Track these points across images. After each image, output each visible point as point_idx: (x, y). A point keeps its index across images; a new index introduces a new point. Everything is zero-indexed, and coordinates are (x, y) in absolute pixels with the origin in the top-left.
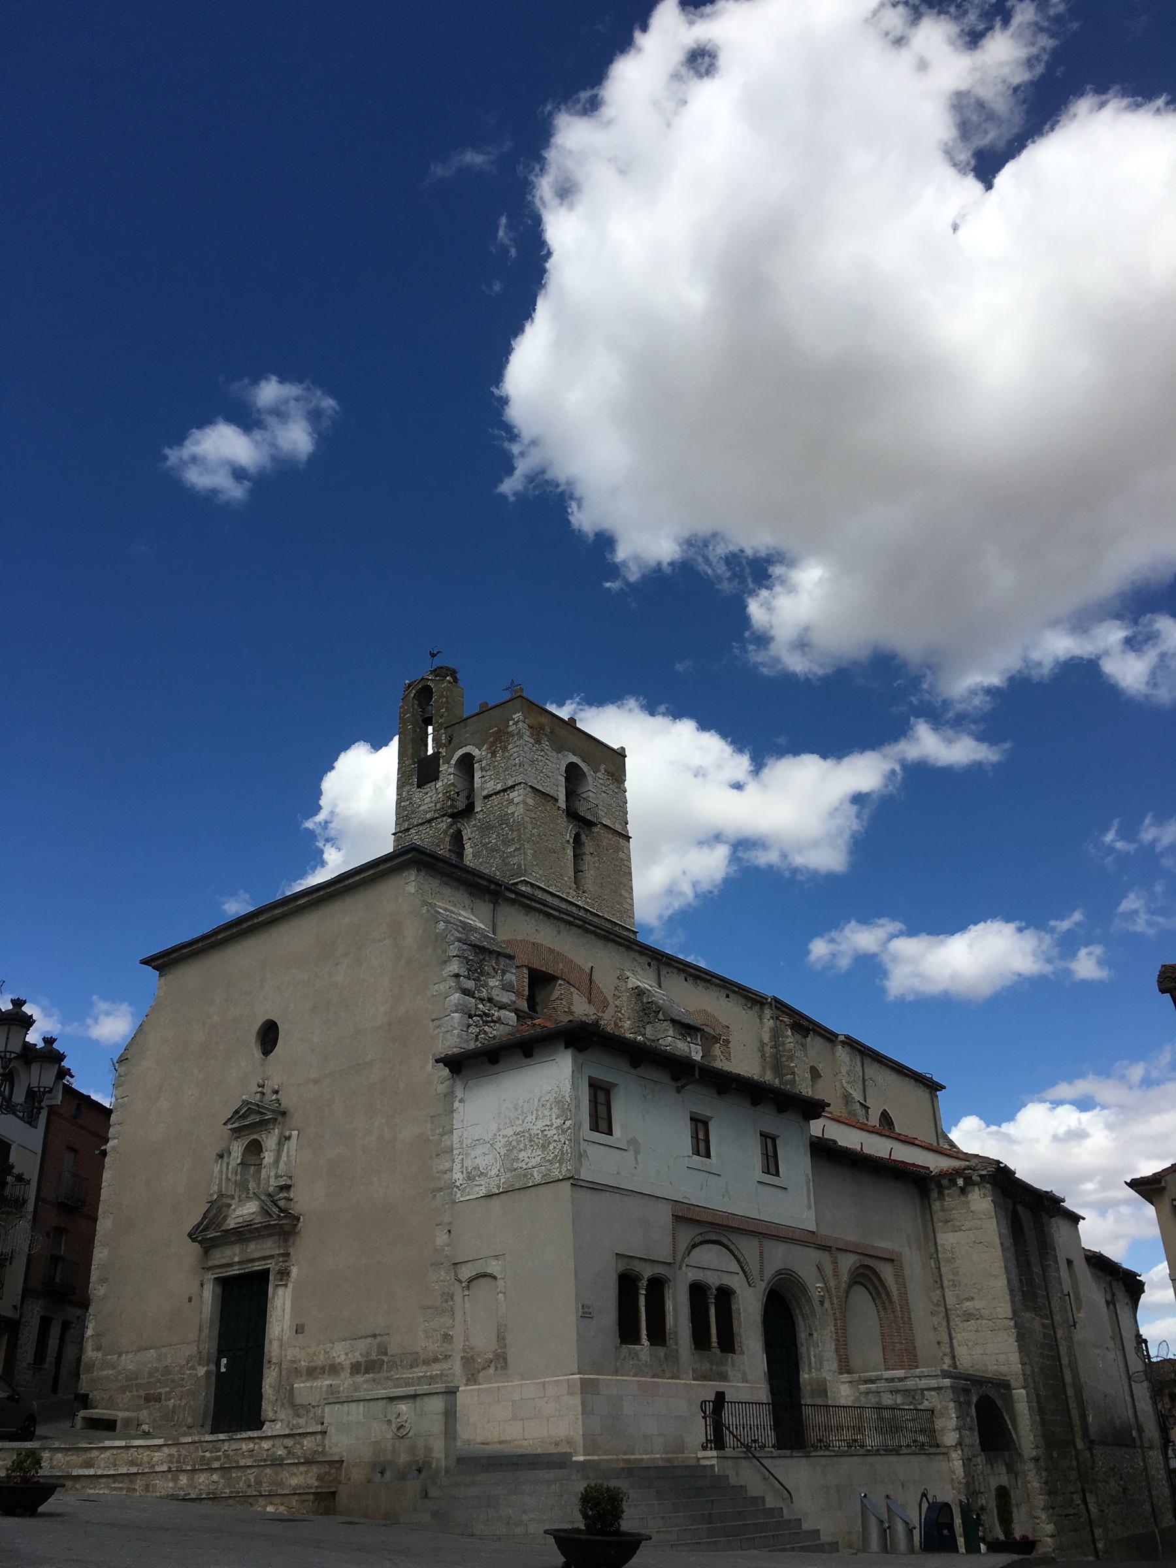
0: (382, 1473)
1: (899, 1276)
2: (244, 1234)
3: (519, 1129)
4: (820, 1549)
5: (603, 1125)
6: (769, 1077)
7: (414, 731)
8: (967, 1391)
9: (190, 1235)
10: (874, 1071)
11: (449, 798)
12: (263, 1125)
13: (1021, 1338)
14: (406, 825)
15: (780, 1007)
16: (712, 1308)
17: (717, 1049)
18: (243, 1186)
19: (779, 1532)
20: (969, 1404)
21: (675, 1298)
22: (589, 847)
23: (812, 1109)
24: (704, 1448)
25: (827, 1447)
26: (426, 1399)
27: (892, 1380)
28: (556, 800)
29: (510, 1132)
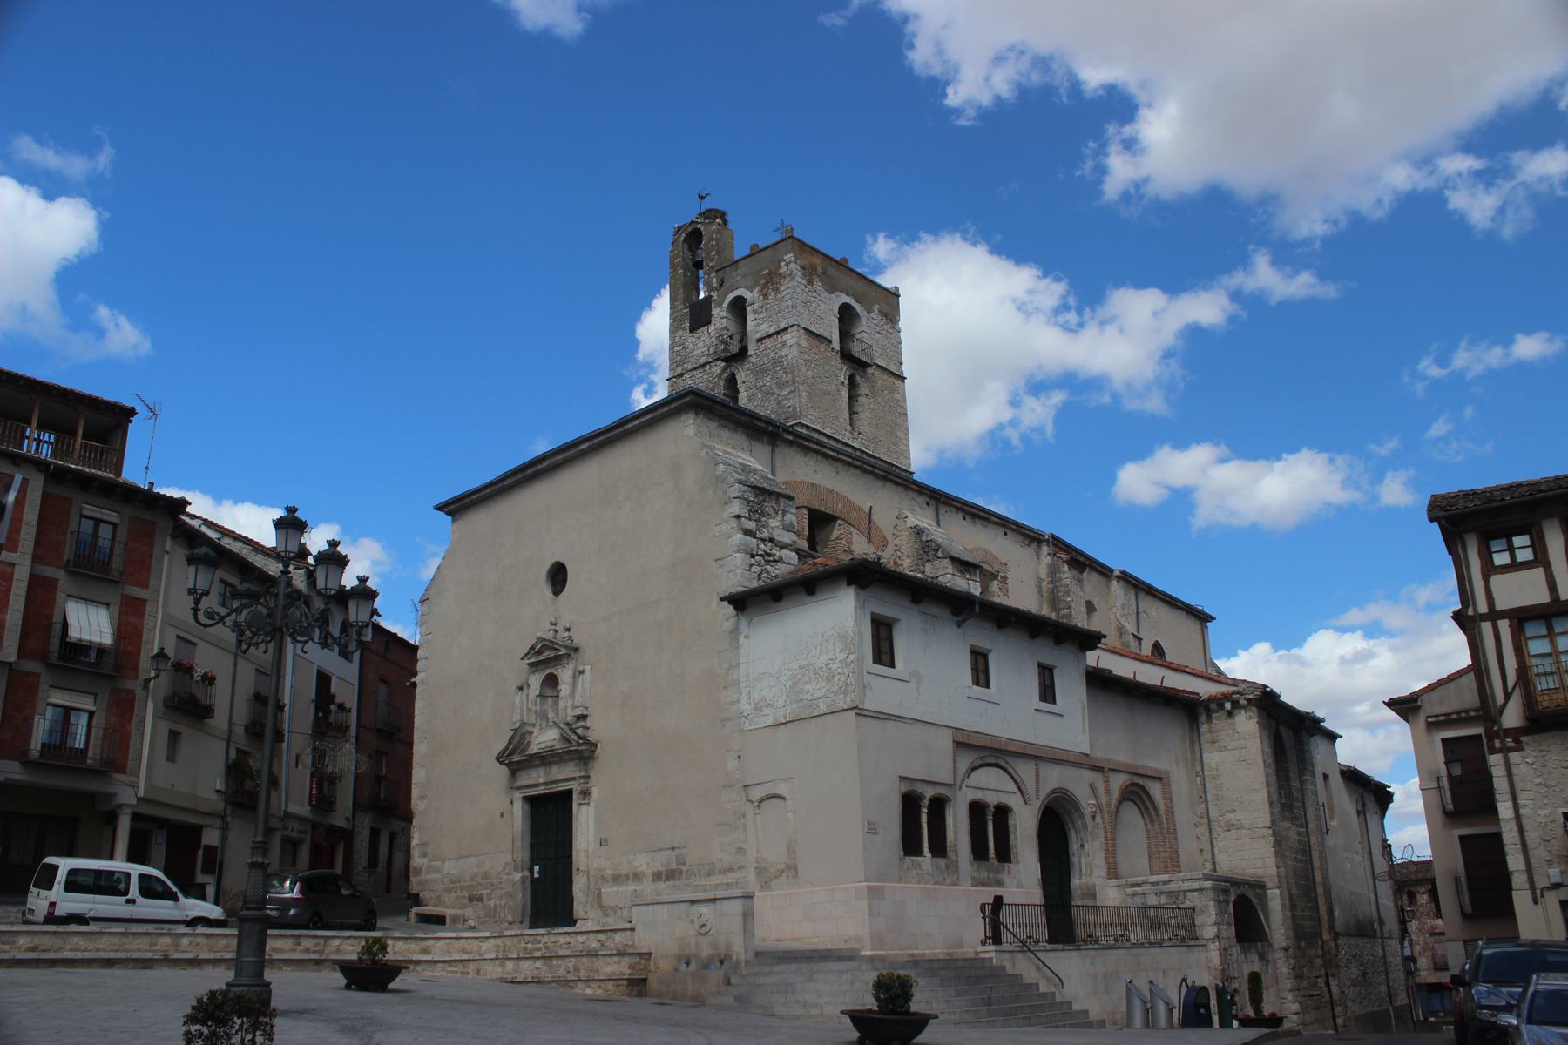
0: (688, 964)
1: (1167, 792)
2: (545, 759)
3: (804, 663)
4: (1089, 1025)
5: (885, 658)
6: (1045, 611)
7: (685, 275)
8: (1226, 892)
9: (497, 759)
10: (1148, 604)
11: (722, 342)
12: (557, 660)
13: (1278, 844)
14: (679, 371)
15: (1058, 544)
16: (990, 826)
17: (995, 586)
18: (543, 716)
19: (1051, 1012)
20: (1227, 902)
21: (955, 816)
22: (863, 389)
23: (1089, 640)
24: (983, 943)
25: (1097, 941)
26: (725, 903)
27: (1157, 883)
28: (830, 341)
29: (794, 665)
